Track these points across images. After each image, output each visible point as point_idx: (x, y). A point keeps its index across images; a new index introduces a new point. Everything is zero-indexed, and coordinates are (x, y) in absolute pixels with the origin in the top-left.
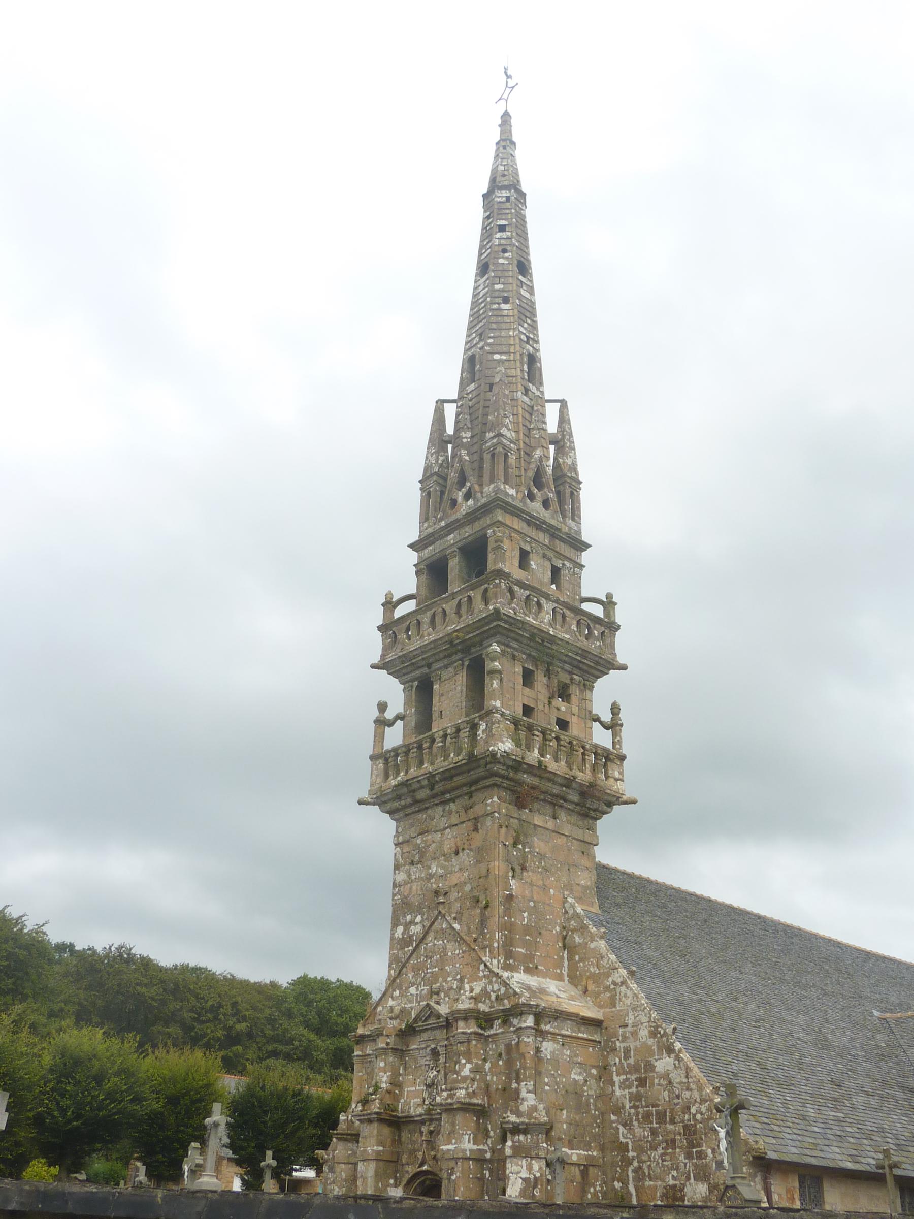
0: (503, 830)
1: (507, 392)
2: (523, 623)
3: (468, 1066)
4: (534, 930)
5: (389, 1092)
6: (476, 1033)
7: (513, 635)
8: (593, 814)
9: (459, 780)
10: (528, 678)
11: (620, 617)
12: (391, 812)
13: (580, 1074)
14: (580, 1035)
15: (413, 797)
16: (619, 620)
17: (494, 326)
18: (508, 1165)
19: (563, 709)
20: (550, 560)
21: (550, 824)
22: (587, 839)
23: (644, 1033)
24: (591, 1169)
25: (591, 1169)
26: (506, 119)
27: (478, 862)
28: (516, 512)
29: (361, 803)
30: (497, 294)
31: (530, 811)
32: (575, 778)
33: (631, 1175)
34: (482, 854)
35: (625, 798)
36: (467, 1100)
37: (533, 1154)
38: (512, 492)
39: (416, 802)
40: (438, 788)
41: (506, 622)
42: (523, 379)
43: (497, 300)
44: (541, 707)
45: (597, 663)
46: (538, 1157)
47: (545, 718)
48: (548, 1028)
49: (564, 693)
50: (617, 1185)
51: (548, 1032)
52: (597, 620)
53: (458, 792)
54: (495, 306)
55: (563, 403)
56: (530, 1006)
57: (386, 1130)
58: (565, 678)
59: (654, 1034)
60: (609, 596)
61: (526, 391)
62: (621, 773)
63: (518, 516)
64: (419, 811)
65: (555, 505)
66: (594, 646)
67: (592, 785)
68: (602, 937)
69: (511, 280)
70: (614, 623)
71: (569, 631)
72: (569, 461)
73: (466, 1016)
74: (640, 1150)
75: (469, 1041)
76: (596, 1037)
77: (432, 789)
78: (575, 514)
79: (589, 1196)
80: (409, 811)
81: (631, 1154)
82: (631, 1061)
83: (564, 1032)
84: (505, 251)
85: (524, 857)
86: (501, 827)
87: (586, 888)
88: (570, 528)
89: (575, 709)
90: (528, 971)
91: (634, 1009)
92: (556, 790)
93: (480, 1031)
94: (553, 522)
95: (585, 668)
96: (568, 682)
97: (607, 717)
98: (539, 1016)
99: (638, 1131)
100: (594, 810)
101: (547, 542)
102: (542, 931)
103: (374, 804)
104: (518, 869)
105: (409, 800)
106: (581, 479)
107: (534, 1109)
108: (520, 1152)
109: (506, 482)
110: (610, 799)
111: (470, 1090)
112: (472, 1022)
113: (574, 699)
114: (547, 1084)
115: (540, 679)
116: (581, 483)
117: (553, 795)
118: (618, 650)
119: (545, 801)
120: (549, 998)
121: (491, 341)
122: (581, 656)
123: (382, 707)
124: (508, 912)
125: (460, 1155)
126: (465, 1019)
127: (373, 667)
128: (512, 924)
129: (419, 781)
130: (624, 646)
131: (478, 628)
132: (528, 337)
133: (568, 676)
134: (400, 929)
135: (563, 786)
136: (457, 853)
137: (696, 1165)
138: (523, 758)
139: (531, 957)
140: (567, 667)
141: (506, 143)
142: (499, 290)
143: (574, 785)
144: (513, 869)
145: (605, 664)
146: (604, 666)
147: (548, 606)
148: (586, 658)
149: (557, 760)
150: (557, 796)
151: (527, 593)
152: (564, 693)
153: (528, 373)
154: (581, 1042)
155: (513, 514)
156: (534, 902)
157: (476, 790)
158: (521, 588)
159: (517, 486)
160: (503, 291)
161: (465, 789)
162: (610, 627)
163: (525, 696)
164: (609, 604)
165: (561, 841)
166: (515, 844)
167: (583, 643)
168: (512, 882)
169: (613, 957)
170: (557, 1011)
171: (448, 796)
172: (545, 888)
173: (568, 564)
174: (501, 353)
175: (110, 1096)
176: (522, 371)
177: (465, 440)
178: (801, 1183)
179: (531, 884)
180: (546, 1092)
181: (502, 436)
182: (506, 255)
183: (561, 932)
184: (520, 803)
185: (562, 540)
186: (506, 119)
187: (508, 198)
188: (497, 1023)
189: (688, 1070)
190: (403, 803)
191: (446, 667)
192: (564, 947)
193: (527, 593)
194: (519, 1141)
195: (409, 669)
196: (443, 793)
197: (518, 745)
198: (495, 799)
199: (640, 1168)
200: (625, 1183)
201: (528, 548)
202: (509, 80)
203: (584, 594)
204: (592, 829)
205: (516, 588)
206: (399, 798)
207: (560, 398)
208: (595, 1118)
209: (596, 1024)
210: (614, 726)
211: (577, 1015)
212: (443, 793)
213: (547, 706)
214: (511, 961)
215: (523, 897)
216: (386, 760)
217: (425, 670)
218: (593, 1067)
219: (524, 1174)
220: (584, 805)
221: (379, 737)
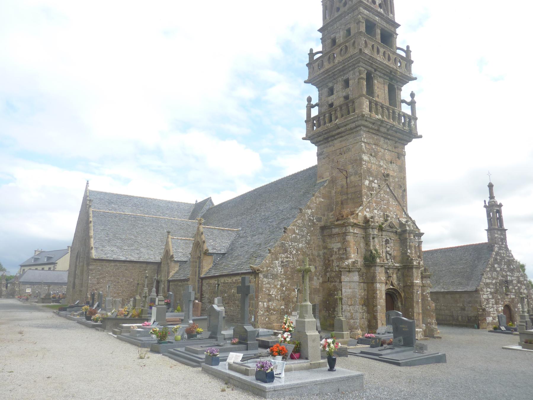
11: (413, 57)
15: (379, 128)
40: (390, 132)
52: (402, 57)
60: (408, 47)
66: (403, 70)
70: (410, 60)
78: (392, 12)
106: (397, 20)
116: (398, 25)
129: (387, 125)
145: (407, 78)
161: (397, 139)
164: (408, 51)
171: (389, 137)
190: (373, 127)
195: (368, 64)
210: (412, 104)
212: (389, 135)
217: (373, 70)
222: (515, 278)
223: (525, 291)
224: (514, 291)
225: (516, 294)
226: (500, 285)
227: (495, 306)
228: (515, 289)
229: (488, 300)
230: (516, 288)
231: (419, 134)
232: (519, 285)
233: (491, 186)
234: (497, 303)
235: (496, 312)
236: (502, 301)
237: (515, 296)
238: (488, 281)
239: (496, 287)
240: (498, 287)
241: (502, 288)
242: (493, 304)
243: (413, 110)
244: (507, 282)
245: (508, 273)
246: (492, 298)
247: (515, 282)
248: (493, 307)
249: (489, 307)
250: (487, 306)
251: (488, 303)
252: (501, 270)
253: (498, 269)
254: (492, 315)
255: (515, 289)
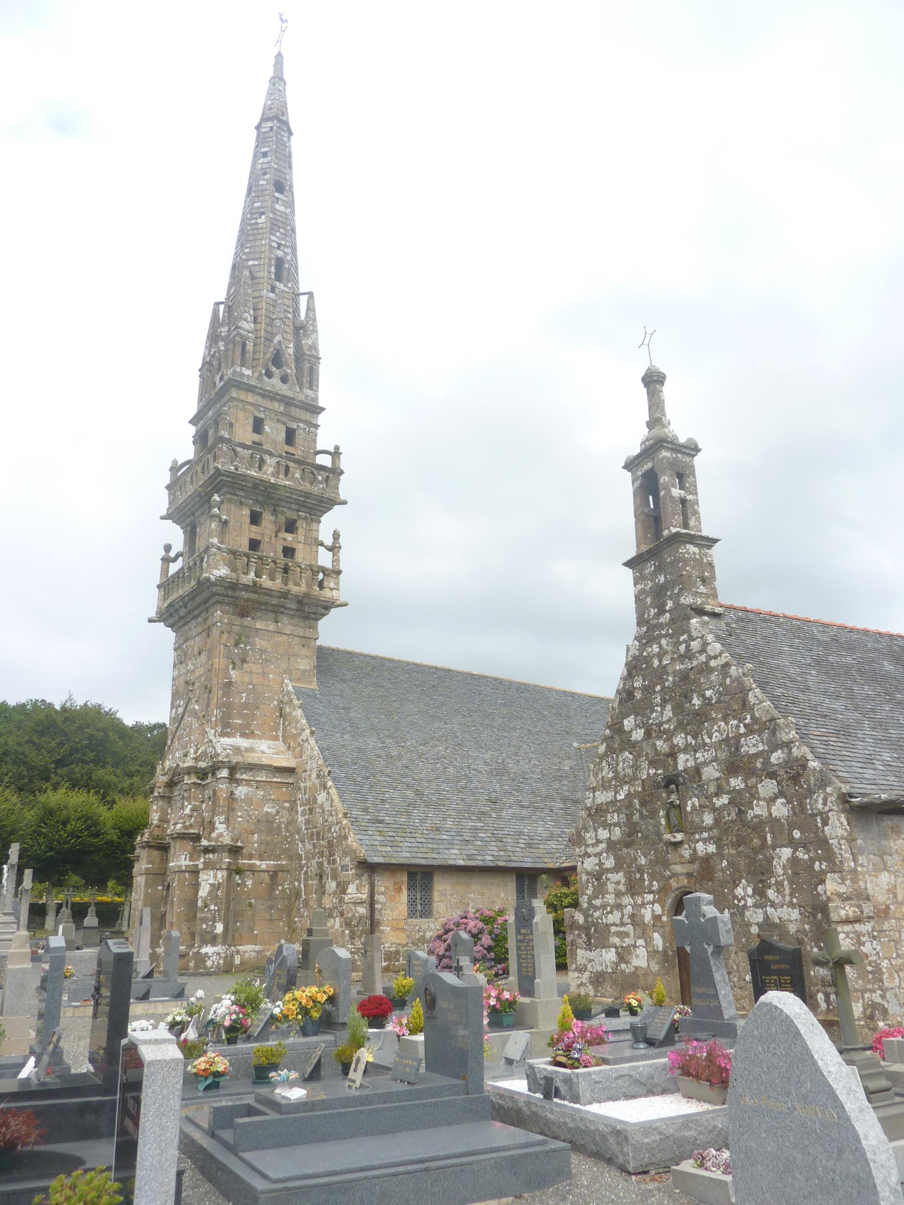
0: (225, 635)
1: (250, 291)
2: (244, 476)
3: (190, 807)
4: (253, 706)
5: (158, 826)
6: (194, 783)
7: (237, 486)
8: (313, 616)
9: (198, 599)
10: (255, 519)
11: (343, 464)
12: (171, 626)
13: (273, 807)
14: (274, 780)
16: (343, 466)
17: (251, 238)
18: (201, 875)
19: (290, 539)
20: (284, 423)
21: (272, 627)
22: (308, 635)
23: (314, 775)
24: (280, 874)
25: (280, 874)
26: (279, 56)
27: (208, 660)
28: (250, 389)
29: (150, 621)
30: (255, 211)
31: (253, 618)
32: (289, 591)
33: (303, 876)
34: (210, 652)
35: (338, 602)
36: (183, 831)
37: (218, 867)
38: (247, 372)
39: (181, 618)
40: (189, 607)
41: (228, 476)
42: (270, 278)
43: (255, 216)
44: (267, 539)
45: (321, 501)
46: (221, 869)
47: (272, 550)
48: (245, 777)
49: (291, 527)
50: (296, 884)
51: (242, 780)
53: (200, 609)
54: (253, 221)
55: (310, 295)
56: (223, 762)
57: (155, 853)
58: (292, 515)
59: (318, 776)
60: (337, 448)
61: (273, 289)
62: (337, 584)
63: (253, 391)
64: (184, 624)
65: (293, 379)
67: (306, 595)
68: (299, 707)
69: (267, 198)
71: (293, 479)
72: (310, 342)
73: (189, 771)
74: (308, 859)
75: (190, 790)
76: (290, 780)
77: (186, 607)
78: (313, 383)
79: (277, 892)
80: (180, 624)
81: (304, 862)
82: (307, 796)
83: (257, 779)
84: (265, 174)
85: (245, 652)
86: (223, 633)
87: (305, 671)
88: (307, 396)
89: (301, 538)
90: (244, 735)
91: (311, 759)
92: (274, 601)
93: (199, 782)
94: (290, 394)
95: (310, 505)
96: (296, 518)
97: (329, 541)
98: (233, 769)
99: (307, 845)
100: (314, 613)
101: (282, 409)
102: (260, 706)
103: (160, 621)
104: (238, 662)
105: (177, 617)
107: (221, 835)
108: (208, 866)
109: (242, 365)
110: (325, 604)
111: (188, 824)
112: (193, 776)
113: (301, 531)
114: (240, 817)
115: (268, 519)
117: (273, 605)
118: (340, 492)
119: (266, 610)
120: (256, 755)
121: (247, 250)
122: (304, 497)
123: (168, 548)
124: (226, 694)
125: (177, 869)
126: (189, 774)
127: (162, 518)
128: (230, 703)
130: (345, 487)
131: (212, 483)
132: (279, 245)
133: (295, 513)
134: (174, 710)
135: (280, 598)
136: (200, 654)
137: (331, 869)
138: (237, 580)
139: (248, 726)
140: (294, 506)
141: (278, 80)
142: (257, 208)
143: (290, 596)
144: (234, 663)
145: (327, 503)
146: (327, 503)
147: (270, 461)
148: (309, 498)
149: (272, 578)
150: (277, 606)
151: (251, 452)
152: (291, 527)
153: (276, 274)
154: (274, 785)
155: (247, 390)
156: (253, 685)
157: (210, 606)
158: (244, 448)
159: (253, 368)
160: (260, 207)
162: (335, 472)
163: (254, 532)
164: (336, 454)
165: (281, 639)
166: (236, 644)
167: (306, 486)
168: (232, 672)
169: (304, 721)
170: (250, 764)
172: (264, 674)
173: (302, 425)
174: (253, 260)
175: (72, 834)
176: (269, 272)
177: (223, 334)
178: (409, 877)
179: (251, 672)
180: (239, 823)
181: (240, 328)
182: (266, 177)
183: (278, 705)
184: (243, 614)
185: (296, 406)
186: (279, 56)
187: (271, 128)
188: (210, 775)
189: (332, 801)
191: (202, 514)
192: (281, 715)
193: (251, 452)
194: (209, 859)
196: (193, 610)
197: (234, 569)
198: (219, 612)
199: (307, 871)
200: (300, 883)
201: (262, 416)
202: (285, 25)
203: (319, 448)
204: (315, 628)
205: (238, 449)
206: (171, 615)
207: (308, 291)
208: (286, 838)
209: (291, 771)
210: (334, 549)
211: (270, 766)
213: (273, 538)
214: (226, 728)
215: (243, 683)
216: (166, 586)
218: (286, 801)
219: (212, 881)
220: (303, 611)
221: (165, 570)
222: (708, 755)
223: (780, 809)
224: (708, 819)
225: (721, 831)
226: (643, 803)
227: (627, 900)
228: (714, 810)
229: (598, 875)
230: (724, 800)
231: (342, 599)
232: (736, 783)
233: (653, 381)
234: (634, 888)
235: (629, 928)
236: (652, 877)
237: (718, 842)
238: (603, 797)
239: (629, 817)
240: (636, 817)
241: (654, 814)
242: (618, 894)
243: (336, 561)
244: (671, 781)
245: (679, 740)
246: (616, 869)
247: (710, 772)
248: (619, 907)
249: (604, 907)
250: (598, 902)
251: (600, 891)
252: (648, 734)
253: (638, 735)
254: (616, 940)
255: (714, 810)
